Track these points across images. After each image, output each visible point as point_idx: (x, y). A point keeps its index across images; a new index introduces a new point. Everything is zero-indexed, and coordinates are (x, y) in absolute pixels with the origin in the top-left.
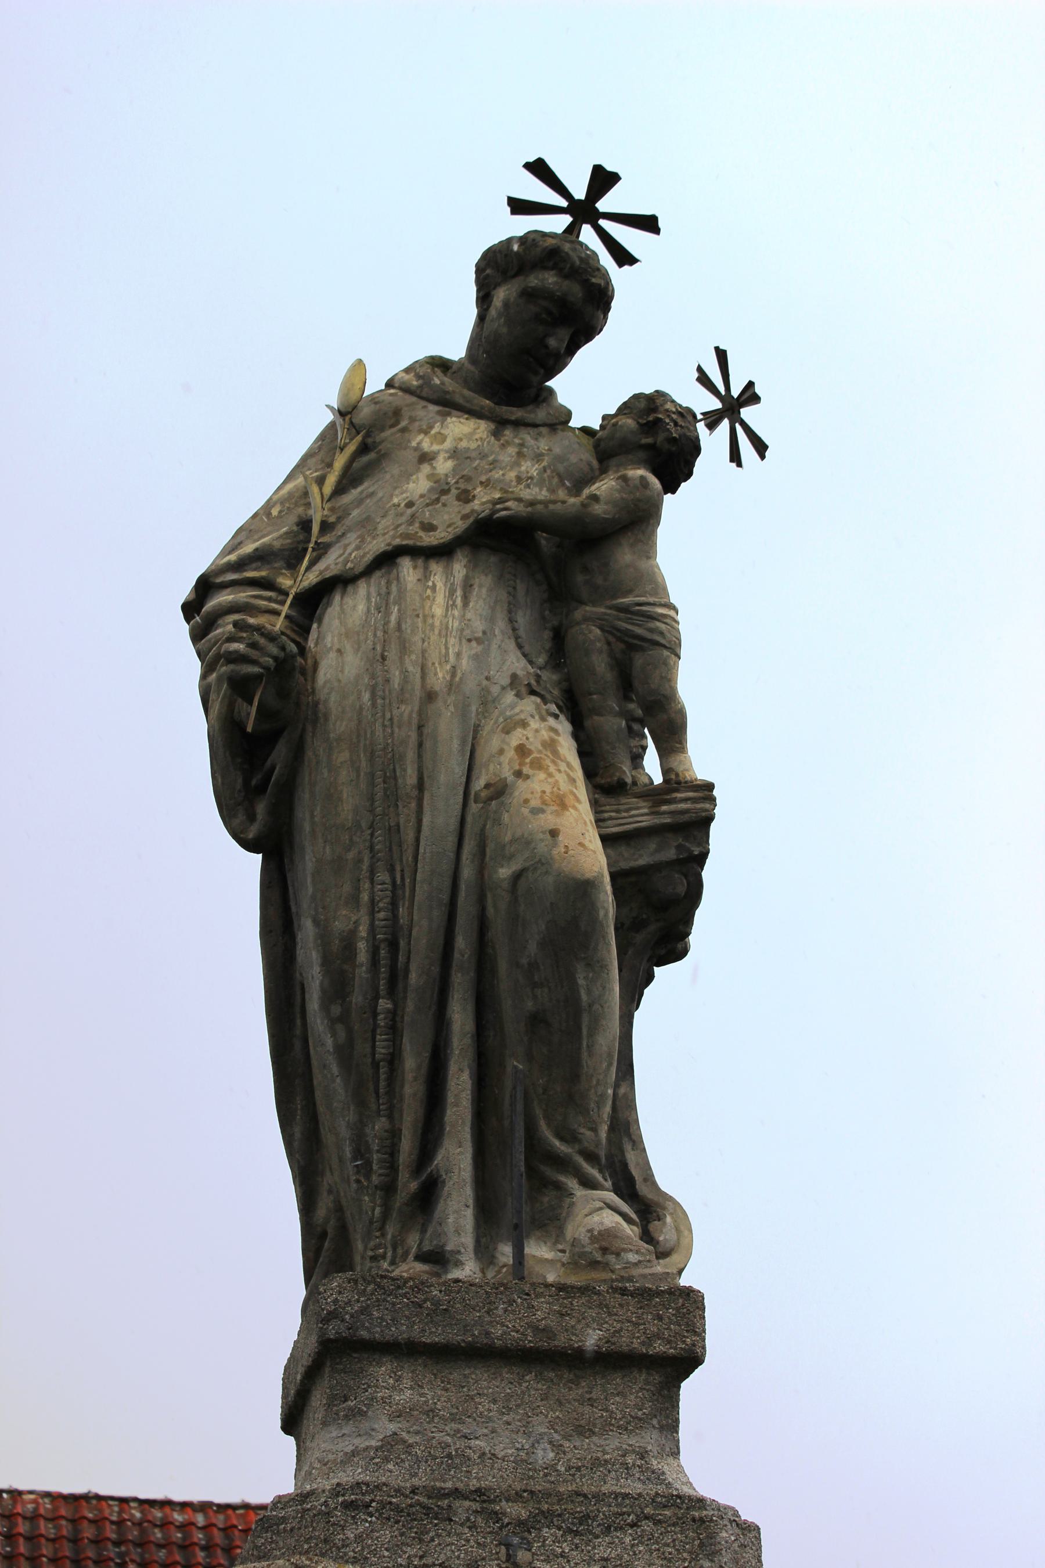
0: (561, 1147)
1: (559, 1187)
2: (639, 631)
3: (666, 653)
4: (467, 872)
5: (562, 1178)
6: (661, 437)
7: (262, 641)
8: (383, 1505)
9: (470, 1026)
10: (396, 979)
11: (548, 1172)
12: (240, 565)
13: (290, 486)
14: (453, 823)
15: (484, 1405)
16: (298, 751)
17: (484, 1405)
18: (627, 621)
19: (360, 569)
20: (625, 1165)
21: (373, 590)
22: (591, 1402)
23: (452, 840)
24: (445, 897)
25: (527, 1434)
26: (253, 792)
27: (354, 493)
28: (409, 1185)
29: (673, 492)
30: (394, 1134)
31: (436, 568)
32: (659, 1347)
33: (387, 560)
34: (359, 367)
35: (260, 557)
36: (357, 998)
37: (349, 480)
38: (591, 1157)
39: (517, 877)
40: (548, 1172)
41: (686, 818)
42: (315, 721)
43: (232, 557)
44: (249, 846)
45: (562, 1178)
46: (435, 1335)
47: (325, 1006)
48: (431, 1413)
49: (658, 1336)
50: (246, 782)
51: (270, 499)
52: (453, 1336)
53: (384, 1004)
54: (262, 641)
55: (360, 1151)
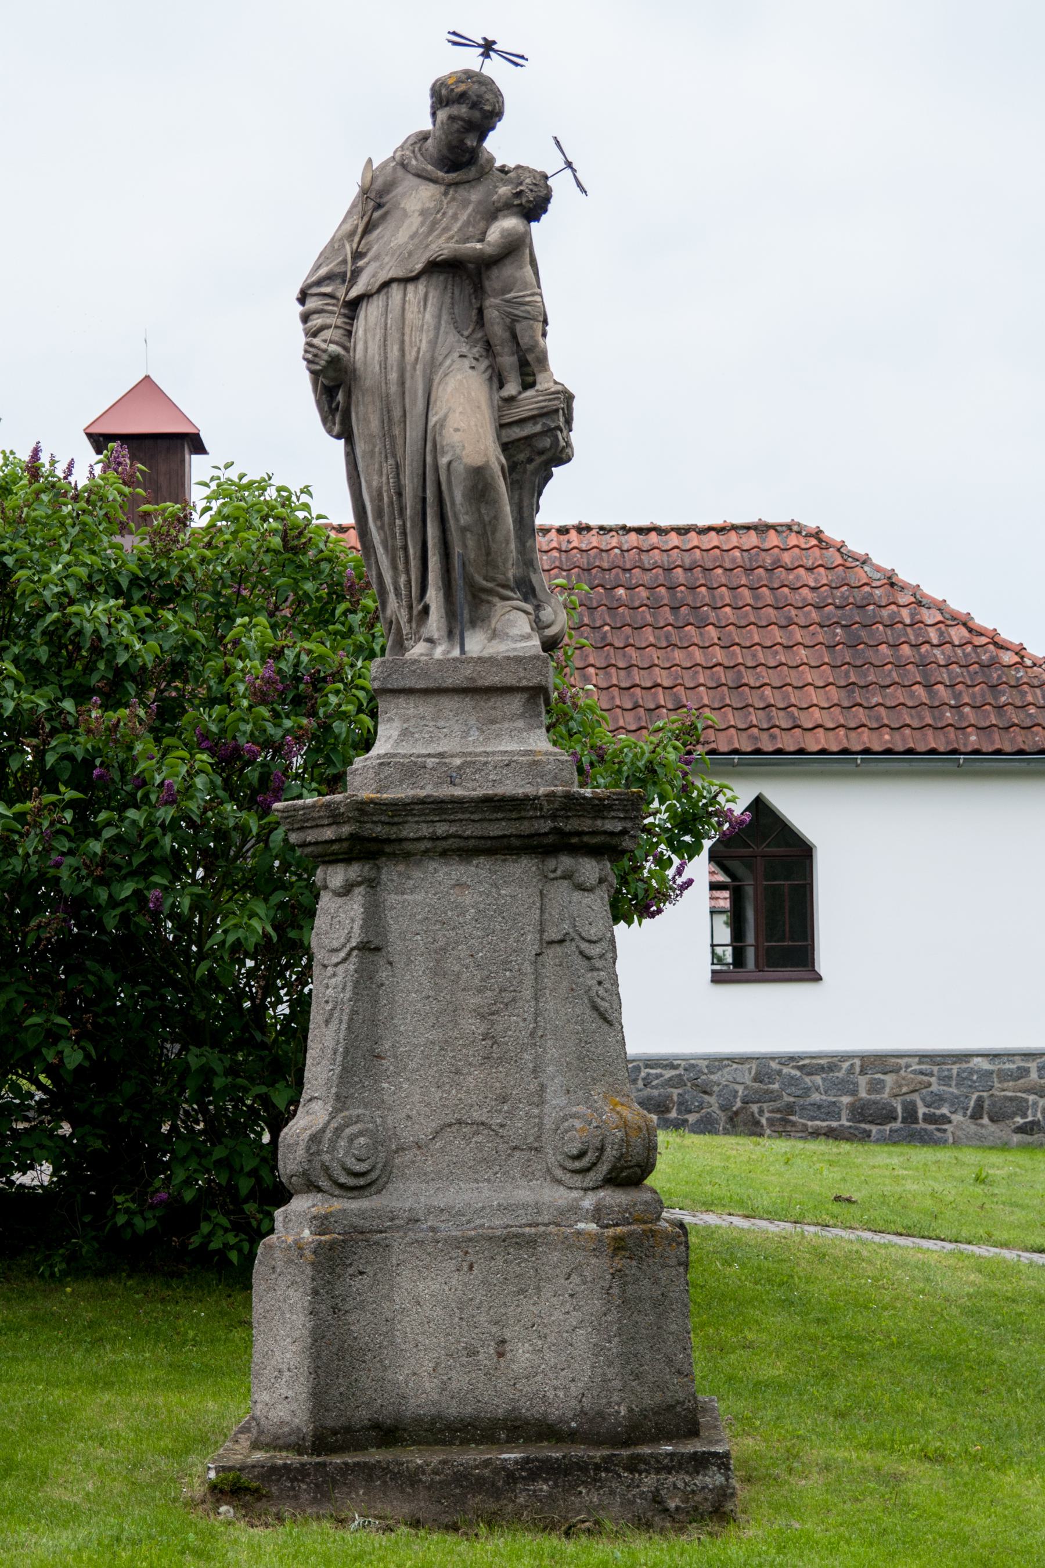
0: (490, 585)
1: (489, 602)
2: (516, 312)
3: (532, 322)
4: (429, 459)
5: (490, 598)
6: (524, 200)
7: (319, 353)
8: (396, 763)
9: (437, 533)
10: (402, 510)
11: (484, 596)
12: (319, 283)
13: (340, 232)
14: (421, 434)
15: (447, 713)
16: (349, 395)
17: (447, 713)
18: (509, 307)
19: (374, 290)
20: (530, 582)
21: (380, 303)
22: (495, 708)
23: (420, 443)
24: (420, 472)
25: (466, 725)
26: (333, 411)
27: (375, 234)
28: (418, 608)
29: (538, 219)
30: (409, 581)
31: (411, 288)
32: (524, 683)
33: (386, 284)
34: (370, 161)
35: (329, 278)
36: (386, 519)
37: (368, 230)
38: (505, 586)
39: (450, 463)
40: (484, 596)
41: (545, 410)
42: (355, 380)
43: (314, 278)
44: (338, 437)
45: (490, 598)
46: (422, 684)
47: (375, 521)
48: (423, 718)
49: (524, 678)
50: (330, 407)
51: (334, 236)
52: (431, 684)
53: (398, 522)
54: (319, 353)
55: (397, 589)
